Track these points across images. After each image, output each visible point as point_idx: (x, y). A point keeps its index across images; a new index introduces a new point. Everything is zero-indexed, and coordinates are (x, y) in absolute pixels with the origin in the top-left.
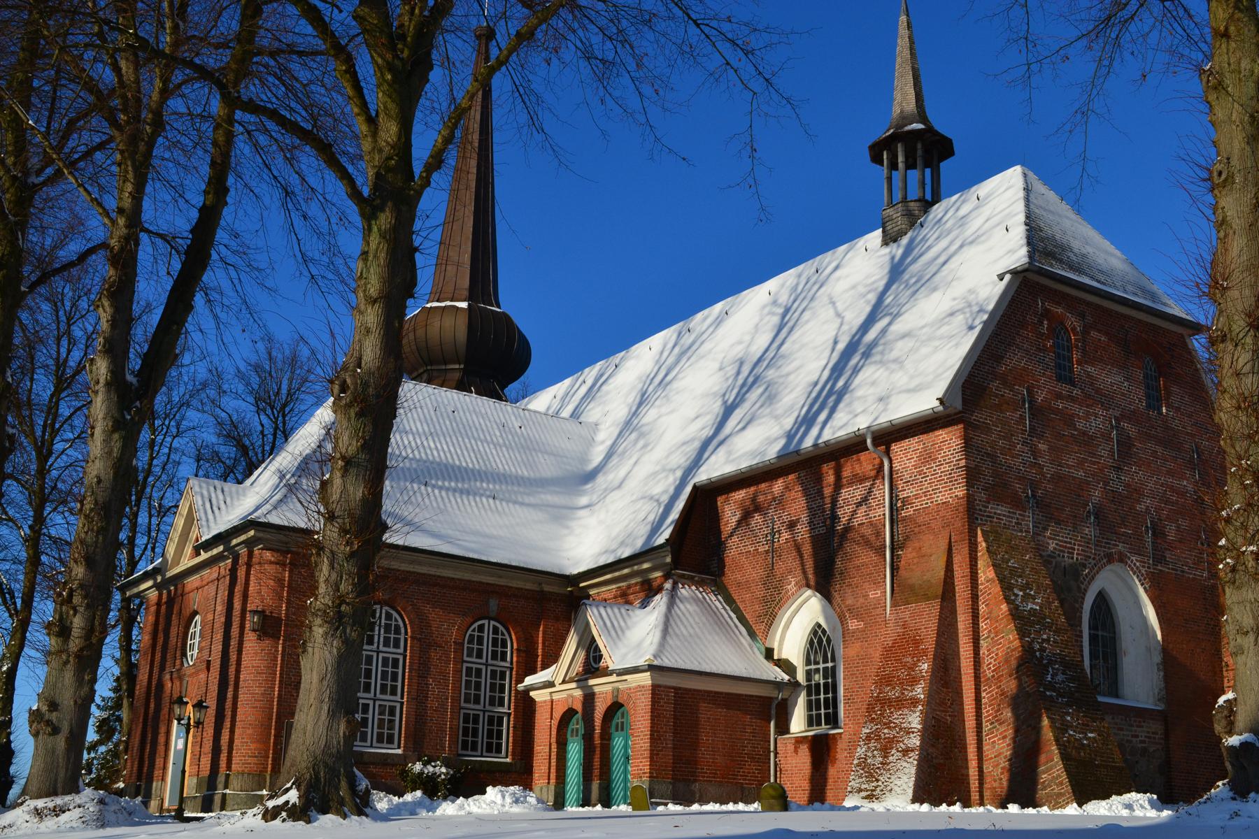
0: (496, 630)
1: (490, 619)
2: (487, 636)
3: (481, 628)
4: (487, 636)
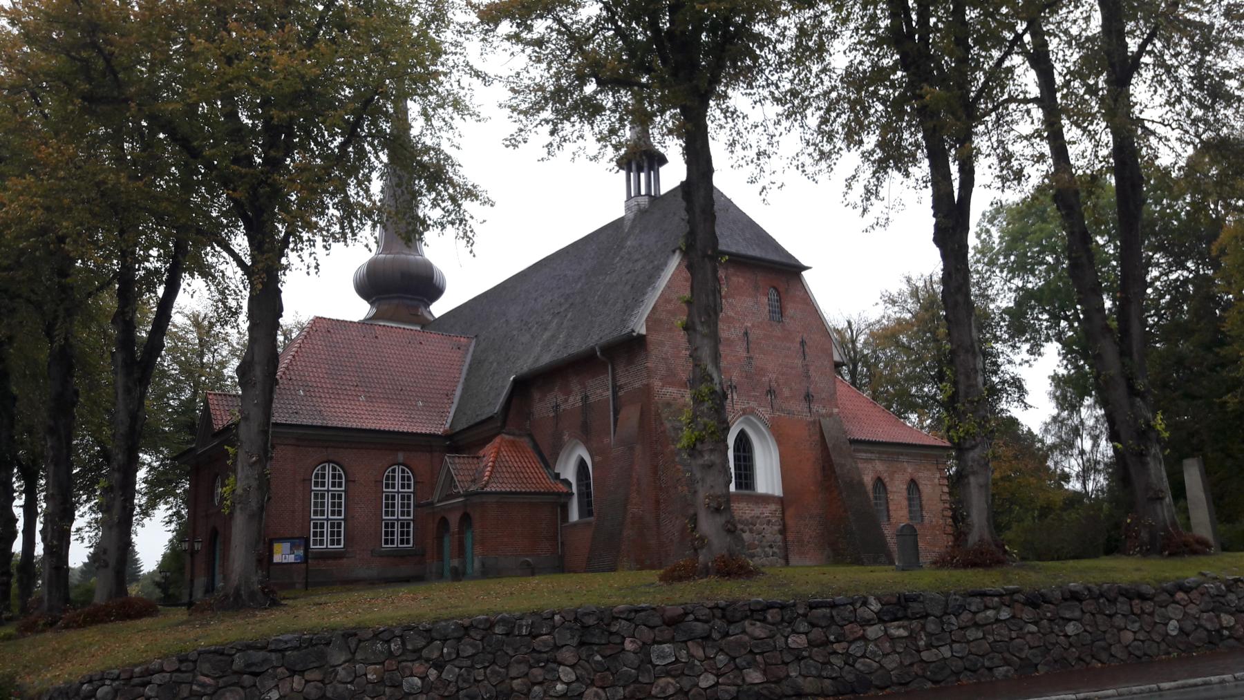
0: (403, 471)
1: (399, 464)
2: (398, 475)
3: (394, 471)
4: (398, 475)
